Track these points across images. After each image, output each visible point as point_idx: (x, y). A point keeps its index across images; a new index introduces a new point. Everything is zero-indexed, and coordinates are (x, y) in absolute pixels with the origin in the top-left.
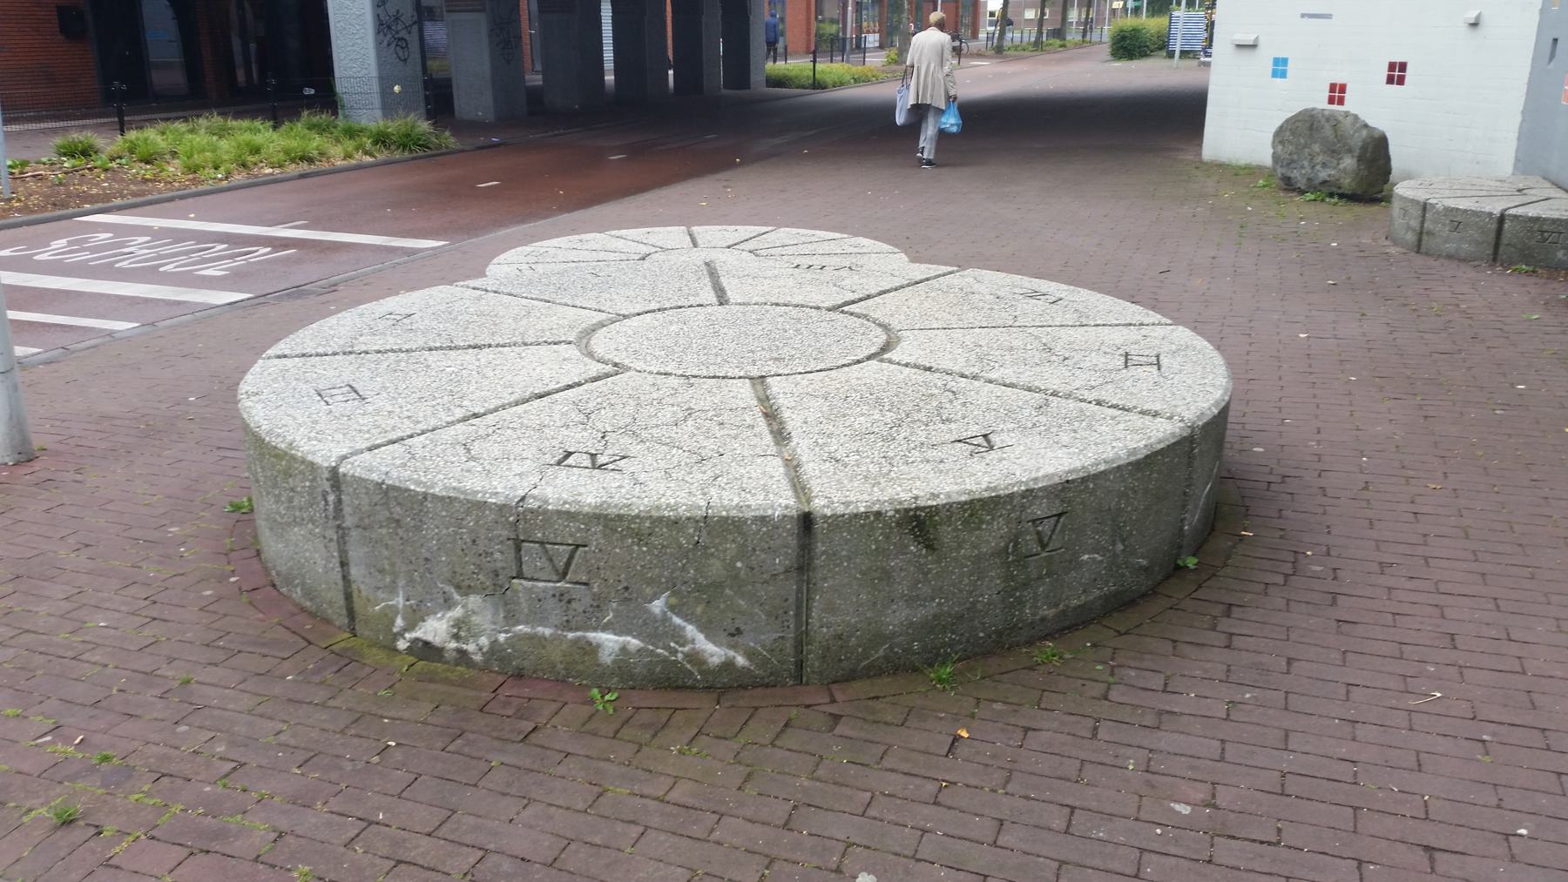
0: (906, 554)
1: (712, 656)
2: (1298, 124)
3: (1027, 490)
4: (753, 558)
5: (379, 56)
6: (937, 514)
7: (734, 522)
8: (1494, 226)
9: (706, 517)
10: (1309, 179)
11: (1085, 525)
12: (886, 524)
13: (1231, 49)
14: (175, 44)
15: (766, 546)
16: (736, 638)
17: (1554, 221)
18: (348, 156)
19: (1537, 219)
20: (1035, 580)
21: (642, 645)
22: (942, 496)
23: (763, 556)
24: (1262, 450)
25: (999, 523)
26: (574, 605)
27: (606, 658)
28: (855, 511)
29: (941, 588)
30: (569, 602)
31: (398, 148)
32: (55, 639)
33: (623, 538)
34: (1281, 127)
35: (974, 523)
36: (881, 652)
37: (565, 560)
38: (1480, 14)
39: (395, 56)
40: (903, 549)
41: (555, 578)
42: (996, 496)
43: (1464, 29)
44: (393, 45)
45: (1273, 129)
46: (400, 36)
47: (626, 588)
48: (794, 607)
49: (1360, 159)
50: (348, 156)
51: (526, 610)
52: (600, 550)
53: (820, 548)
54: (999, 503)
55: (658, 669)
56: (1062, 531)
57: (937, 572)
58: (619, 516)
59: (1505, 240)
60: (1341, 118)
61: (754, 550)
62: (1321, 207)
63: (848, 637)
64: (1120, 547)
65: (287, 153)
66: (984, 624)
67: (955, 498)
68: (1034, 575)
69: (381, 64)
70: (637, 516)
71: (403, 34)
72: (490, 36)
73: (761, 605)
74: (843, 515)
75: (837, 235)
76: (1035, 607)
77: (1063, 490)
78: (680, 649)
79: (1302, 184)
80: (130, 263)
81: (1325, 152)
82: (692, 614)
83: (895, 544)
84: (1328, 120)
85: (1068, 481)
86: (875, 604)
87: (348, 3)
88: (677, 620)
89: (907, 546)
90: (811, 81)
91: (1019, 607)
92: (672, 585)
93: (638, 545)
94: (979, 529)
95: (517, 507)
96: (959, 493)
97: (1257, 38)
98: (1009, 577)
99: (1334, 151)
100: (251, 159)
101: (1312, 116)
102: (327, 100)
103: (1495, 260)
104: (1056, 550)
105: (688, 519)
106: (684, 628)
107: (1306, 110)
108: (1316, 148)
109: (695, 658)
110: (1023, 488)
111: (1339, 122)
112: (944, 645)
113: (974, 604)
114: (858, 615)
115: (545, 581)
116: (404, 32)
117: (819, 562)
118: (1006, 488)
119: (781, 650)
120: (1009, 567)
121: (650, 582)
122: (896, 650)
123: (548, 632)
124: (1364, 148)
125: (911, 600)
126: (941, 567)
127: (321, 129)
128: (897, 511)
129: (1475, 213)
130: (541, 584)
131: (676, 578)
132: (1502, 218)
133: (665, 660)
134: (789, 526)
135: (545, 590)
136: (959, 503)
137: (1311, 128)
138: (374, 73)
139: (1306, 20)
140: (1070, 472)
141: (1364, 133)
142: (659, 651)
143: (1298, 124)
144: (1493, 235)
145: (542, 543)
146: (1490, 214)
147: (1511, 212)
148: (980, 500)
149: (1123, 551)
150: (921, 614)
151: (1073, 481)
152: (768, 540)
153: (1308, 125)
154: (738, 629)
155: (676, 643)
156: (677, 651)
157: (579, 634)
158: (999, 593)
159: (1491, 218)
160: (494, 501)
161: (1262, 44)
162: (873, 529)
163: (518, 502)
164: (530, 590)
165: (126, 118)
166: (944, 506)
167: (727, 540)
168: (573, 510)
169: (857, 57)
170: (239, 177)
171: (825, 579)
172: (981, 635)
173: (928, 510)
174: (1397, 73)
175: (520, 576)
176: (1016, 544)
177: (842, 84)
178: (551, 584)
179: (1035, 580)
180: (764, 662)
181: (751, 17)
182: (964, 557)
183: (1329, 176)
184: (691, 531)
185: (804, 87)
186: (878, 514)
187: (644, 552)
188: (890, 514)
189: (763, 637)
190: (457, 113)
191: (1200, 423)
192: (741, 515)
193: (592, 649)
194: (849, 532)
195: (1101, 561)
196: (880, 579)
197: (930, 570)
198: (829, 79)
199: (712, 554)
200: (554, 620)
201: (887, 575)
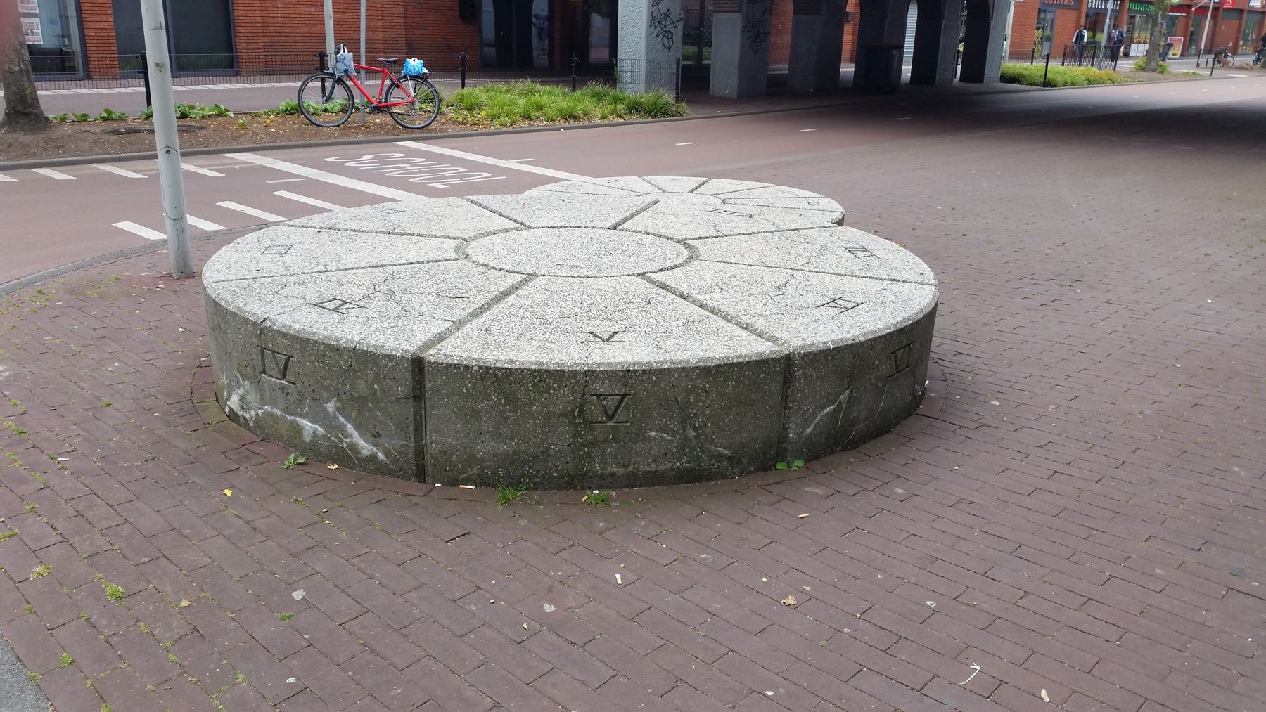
0: (490, 401)
1: (363, 449)
3: (589, 371)
4: (384, 383)
5: (648, 44)
6: (511, 375)
7: (371, 355)
9: (354, 349)
11: (650, 408)
12: (472, 375)
15: (392, 377)
16: (377, 439)
18: (604, 117)
20: (602, 442)
21: (324, 432)
22: (517, 363)
23: (391, 383)
24: (998, 403)
25: (565, 392)
26: (289, 397)
27: (307, 437)
28: (450, 362)
29: (518, 432)
30: (287, 394)
31: (646, 113)
32: (80, 372)
33: (310, 355)
35: (543, 387)
36: (475, 471)
37: (283, 365)
39: (661, 44)
40: (487, 397)
41: (279, 376)
42: (561, 370)
44: (661, 36)
46: (667, 29)
47: (314, 391)
48: (413, 425)
50: (604, 117)
51: (268, 397)
52: (299, 362)
53: (428, 385)
54: (564, 376)
55: (333, 451)
56: (627, 408)
57: (514, 419)
58: (307, 339)
61: (384, 377)
63: (451, 454)
64: (692, 433)
65: (560, 110)
66: (557, 467)
67: (527, 366)
68: (601, 437)
69: (649, 50)
70: (316, 342)
71: (670, 27)
72: (743, 31)
73: (391, 418)
74: (442, 364)
75: (765, 185)
76: (603, 462)
77: (624, 376)
78: (345, 440)
80: (420, 180)
82: (350, 416)
83: (480, 392)
85: (629, 371)
86: (468, 433)
87: (632, 2)
88: (342, 419)
89: (489, 395)
90: (1042, 80)
91: (588, 460)
92: (338, 395)
93: (318, 361)
94: (548, 392)
95: (260, 325)
96: (532, 363)
98: (576, 435)
100: (534, 113)
102: (607, 72)
104: (622, 422)
105: (344, 348)
106: (346, 425)
109: (353, 447)
110: (586, 368)
112: (523, 475)
113: (547, 449)
114: (457, 440)
115: (275, 378)
116: (672, 26)
117: (429, 394)
118: (572, 366)
119: (406, 454)
120: (576, 428)
121: (327, 389)
122: (486, 471)
123: (279, 413)
125: (496, 436)
126: (517, 416)
127: (598, 97)
128: (480, 367)
130: (274, 379)
131: (340, 389)
133: (337, 446)
134: (406, 365)
135: (275, 384)
136: (529, 370)
138: (643, 56)
140: (634, 364)
142: (333, 438)
145: (273, 352)
148: (546, 371)
149: (696, 438)
150: (502, 448)
151: (635, 371)
152: (393, 372)
154: (378, 433)
155: (342, 435)
156: (343, 441)
157: (293, 417)
158: (569, 445)
160: (251, 318)
162: (463, 378)
163: (262, 322)
164: (269, 382)
166: (517, 370)
167: (367, 367)
168: (285, 331)
170: (523, 124)
171: (433, 408)
172: (555, 474)
173: (503, 371)
175: (264, 372)
176: (581, 411)
177: (1073, 84)
178: (278, 381)
179: (602, 442)
180: (395, 461)
181: (992, 23)
182: (536, 411)
184: (346, 357)
185: (1036, 85)
186: (467, 367)
187: (321, 367)
188: (476, 368)
189: (394, 442)
190: (711, 92)
191: (802, 352)
192: (375, 351)
193: (298, 430)
194: (447, 376)
195: (672, 441)
196: (471, 416)
197: (508, 417)
198: (1059, 79)
199: (359, 376)
200: (281, 405)
201: (476, 414)
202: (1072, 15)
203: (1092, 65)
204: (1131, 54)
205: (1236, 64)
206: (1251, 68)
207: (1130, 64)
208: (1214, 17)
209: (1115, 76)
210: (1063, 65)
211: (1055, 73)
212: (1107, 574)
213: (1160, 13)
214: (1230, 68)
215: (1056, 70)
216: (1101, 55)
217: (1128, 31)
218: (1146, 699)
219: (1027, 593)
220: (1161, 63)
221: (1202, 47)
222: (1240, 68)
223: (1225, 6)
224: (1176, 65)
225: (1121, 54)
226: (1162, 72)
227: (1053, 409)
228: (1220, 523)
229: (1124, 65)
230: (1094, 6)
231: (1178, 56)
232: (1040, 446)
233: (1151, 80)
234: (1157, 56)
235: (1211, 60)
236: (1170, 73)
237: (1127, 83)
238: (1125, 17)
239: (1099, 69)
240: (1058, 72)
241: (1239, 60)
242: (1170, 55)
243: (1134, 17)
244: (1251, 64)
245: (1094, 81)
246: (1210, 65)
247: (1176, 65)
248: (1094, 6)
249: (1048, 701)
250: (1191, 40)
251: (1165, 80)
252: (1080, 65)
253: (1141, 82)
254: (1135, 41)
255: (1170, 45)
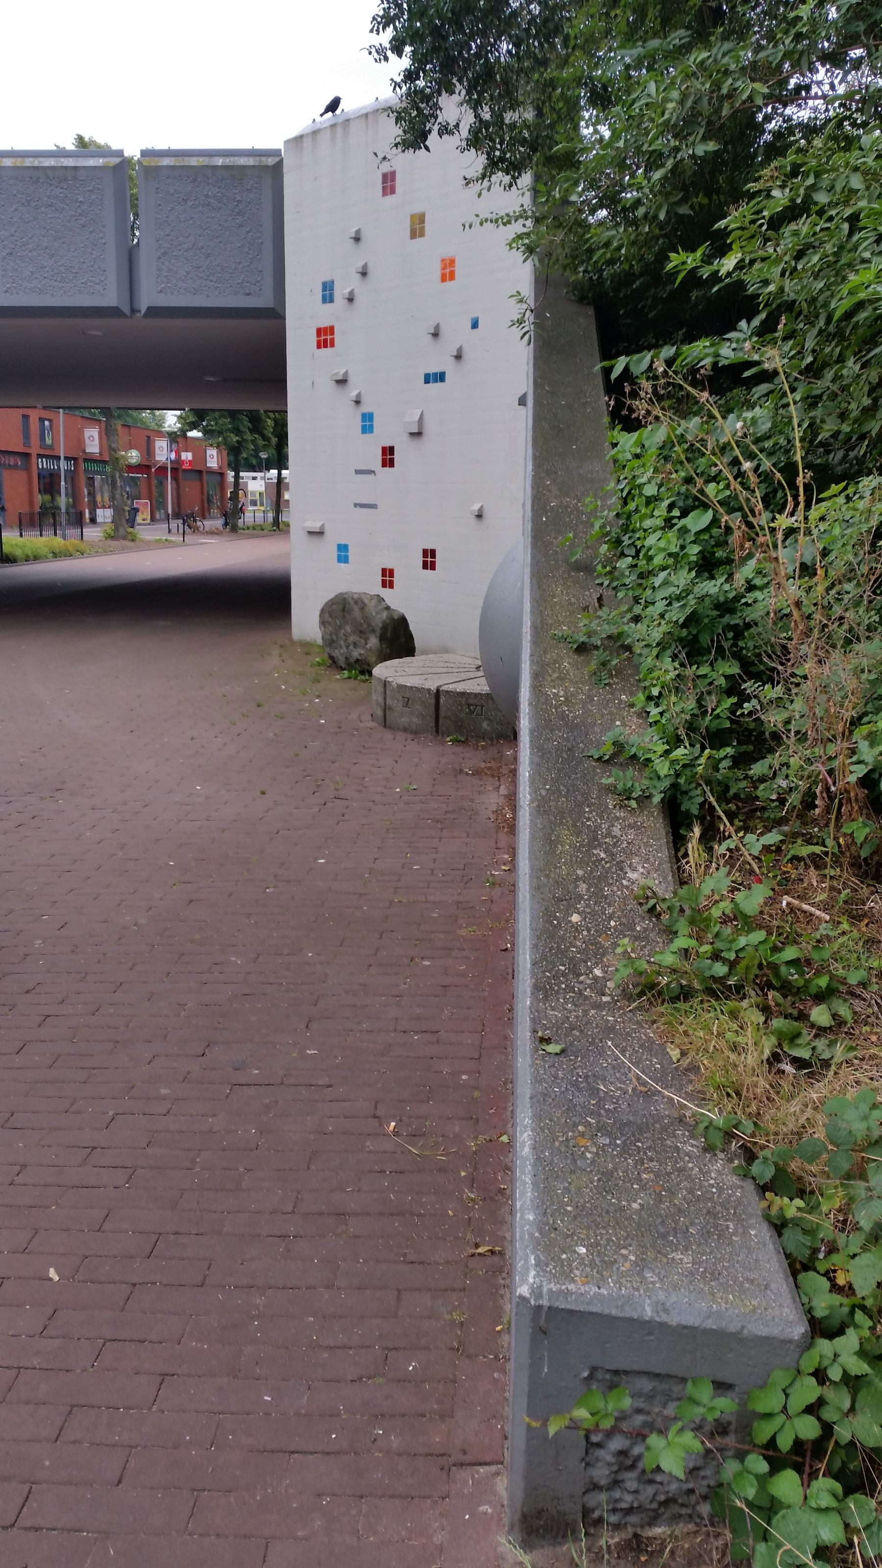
2: (334, 607)
8: (432, 701)
10: (347, 658)
13: (304, 536)
14: (34, 415)
17: (476, 695)
19: (463, 694)
34: (322, 609)
38: (482, 506)
43: (472, 519)
45: (320, 607)
49: (382, 638)
59: (442, 714)
60: (366, 601)
62: (353, 683)
79: (342, 662)
81: (355, 633)
84: (356, 602)
97: (323, 525)
99: (361, 632)
101: (344, 599)
103: (437, 731)
107: (341, 594)
108: (348, 629)
111: (365, 604)
124: (384, 628)
129: (419, 690)
132: (438, 693)
137: (344, 610)
139: (359, 509)
141: (385, 615)
143: (334, 607)
144: (433, 709)
146: (429, 690)
147: (445, 688)
153: (341, 607)
159: (430, 694)
161: (328, 530)
165: (241, 474)
169: (75, 531)
174: (429, 559)
177: (36, 558)
183: (360, 654)
198: (18, 552)
202: (22, 475)
203: (55, 534)
204: (98, 520)
205: (207, 529)
206: (221, 532)
207: (98, 532)
208: (175, 478)
209: (82, 546)
210: (41, 535)
211: (12, 546)
212: (111, 1113)
213: (117, 475)
214: (202, 533)
215: (14, 543)
216: (64, 523)
217: (89, 494)
218: (160, 1234)
219: (24, 1166)
220: (130, 530)
221: (170, 511)
222: (211, 533)
223: (184, 467)
224: (146, 532)
225: (88, 521)
226: (133, 540)
227: (40, 944)
228: (221, 1020)
229: (92, 533)
230: (45, 466)
231: (149, 521)
232: (27, 992)
233: (123, 549)
234: (124, 522)
235: (181, 526)
236: (142, 541)
237: (97, 554)
238: (82, 479)
239: (65, 539)
240: (16, 545)
241: (209, 524)
242: (139, 519)
243: (92, 478)
244: (221, 528)
245: (60, 552)
246: (181, 531)
247: (146, 532)
248: (45, 466)
249: (58, 1278)
250: (158, 505)
251: (138, 549)
252: (41, 535)
253: (112, 552)
254: (100, 505)
255: (136, 510)
